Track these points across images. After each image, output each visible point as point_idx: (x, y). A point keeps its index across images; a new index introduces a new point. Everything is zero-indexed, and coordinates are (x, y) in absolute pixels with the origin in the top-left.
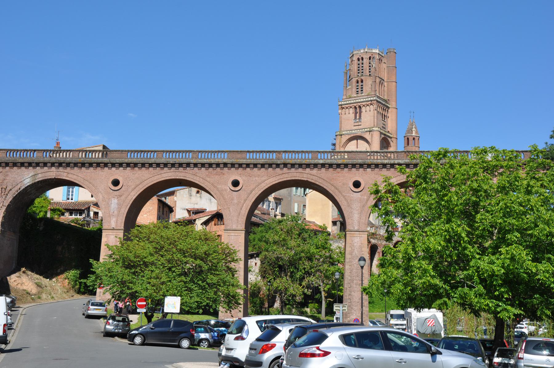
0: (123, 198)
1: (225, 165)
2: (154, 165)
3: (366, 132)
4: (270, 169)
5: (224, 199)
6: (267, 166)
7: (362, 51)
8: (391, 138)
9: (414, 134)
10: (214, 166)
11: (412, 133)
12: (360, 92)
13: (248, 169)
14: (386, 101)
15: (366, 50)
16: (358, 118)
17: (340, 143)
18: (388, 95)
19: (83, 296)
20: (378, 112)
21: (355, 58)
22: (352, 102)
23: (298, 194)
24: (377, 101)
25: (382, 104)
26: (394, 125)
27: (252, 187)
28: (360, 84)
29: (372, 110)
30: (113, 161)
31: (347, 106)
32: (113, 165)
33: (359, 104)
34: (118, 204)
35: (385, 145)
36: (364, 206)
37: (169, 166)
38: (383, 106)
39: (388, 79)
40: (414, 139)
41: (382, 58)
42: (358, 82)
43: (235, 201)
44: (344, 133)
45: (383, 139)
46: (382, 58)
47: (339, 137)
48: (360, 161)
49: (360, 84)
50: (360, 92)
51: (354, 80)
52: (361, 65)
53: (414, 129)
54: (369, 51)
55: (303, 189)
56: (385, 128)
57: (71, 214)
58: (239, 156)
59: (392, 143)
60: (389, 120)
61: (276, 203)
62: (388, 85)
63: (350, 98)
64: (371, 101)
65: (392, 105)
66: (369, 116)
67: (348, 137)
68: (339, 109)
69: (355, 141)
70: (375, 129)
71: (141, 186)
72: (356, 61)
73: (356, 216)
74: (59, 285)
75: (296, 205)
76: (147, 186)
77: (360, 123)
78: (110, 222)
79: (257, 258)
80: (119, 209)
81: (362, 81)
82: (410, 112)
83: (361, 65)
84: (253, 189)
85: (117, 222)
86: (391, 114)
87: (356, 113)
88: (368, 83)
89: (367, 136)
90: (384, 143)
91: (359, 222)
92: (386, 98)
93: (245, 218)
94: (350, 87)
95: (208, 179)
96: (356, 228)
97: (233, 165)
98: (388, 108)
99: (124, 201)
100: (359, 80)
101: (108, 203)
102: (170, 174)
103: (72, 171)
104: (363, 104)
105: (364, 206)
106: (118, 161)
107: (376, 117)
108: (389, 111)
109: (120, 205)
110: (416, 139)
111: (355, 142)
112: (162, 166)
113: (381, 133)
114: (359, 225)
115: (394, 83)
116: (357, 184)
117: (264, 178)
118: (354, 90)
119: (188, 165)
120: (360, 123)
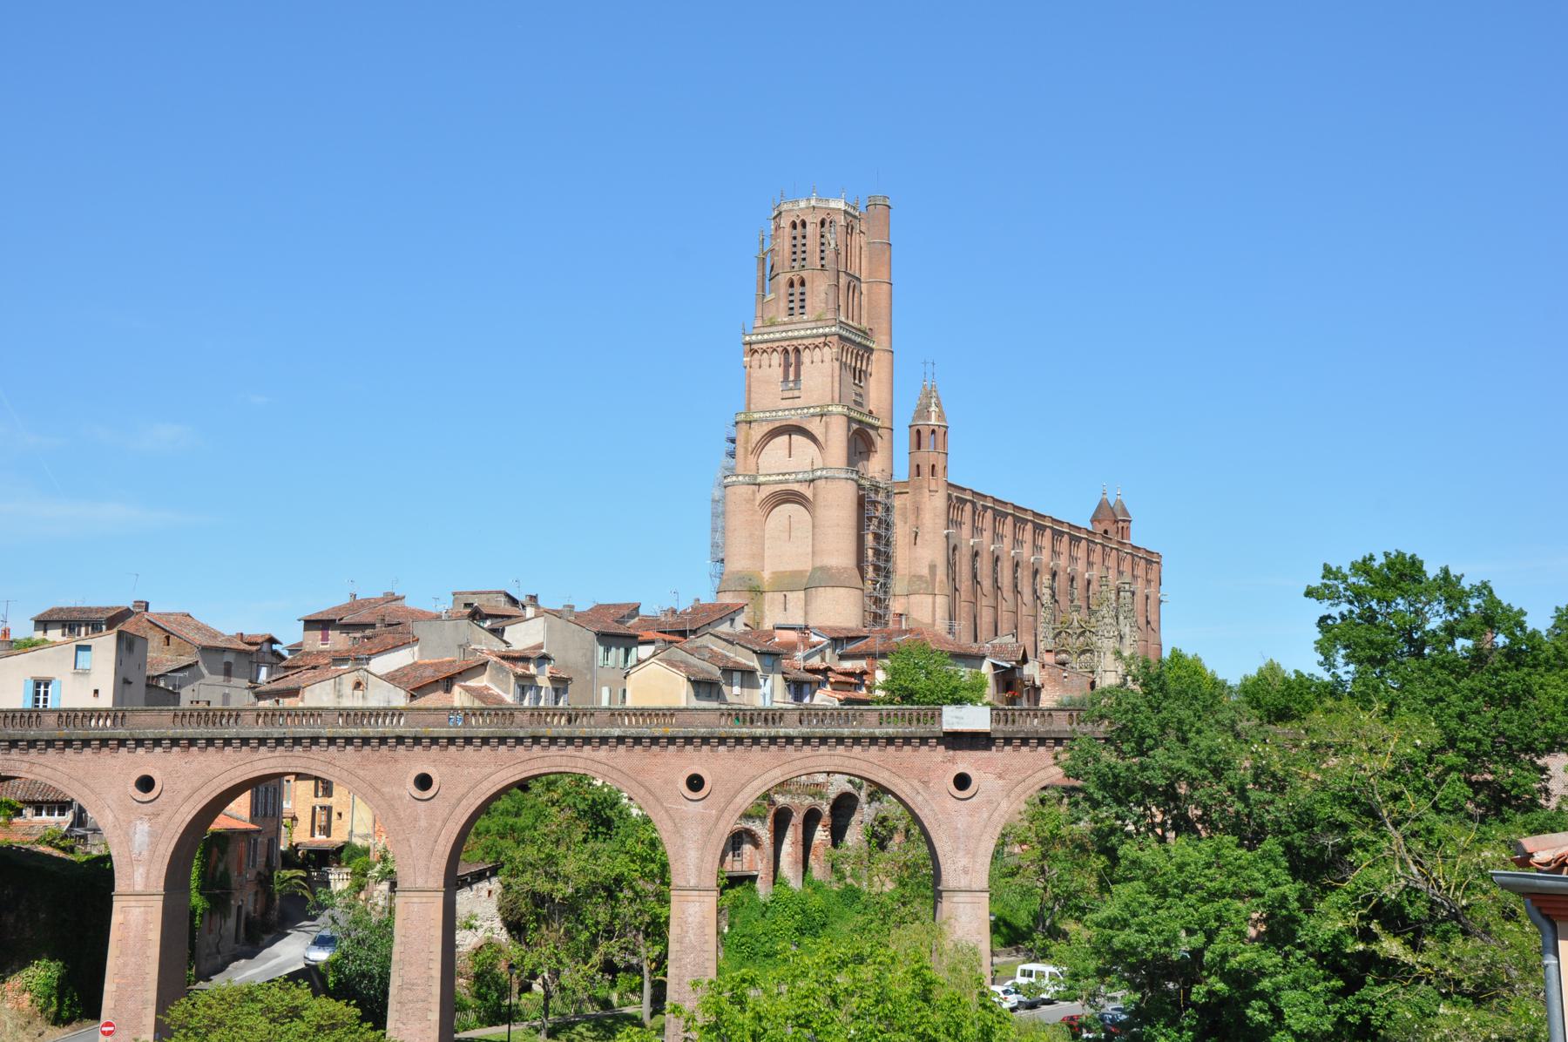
0: (161, 819)
1: (400, 740)
2: (236, 743)
3: (813, 415)
4: (502, 748)
5: (398, 818)
6: (494, 742)
7: (803, 204)
8: (876, 428)
9: (933, 421)
10: (375, 742)
11: (929, 418)
12: (797, 310)
13: (452, 749)
14: (865, 333)
15: (813, 203)
16: (792, 378)
17: (747, 442)
18: (870, 318)
19: (67, 1029)
20: (843, 365)
21: (785, 223)
22: (778, 336)
23: (611, 662)
24: (841, 337)
25: (853, 342)
26: (885, 395)
27: (462, 790)
28: (798, 289)
29: (827, 358)
30: (138, 733)
31: (764, 346)
32: (140, 742)
33: (795, 343)
34: (152, 834)
35: (861, 447)
36: (709, 833)
37: (271, 743)
38: (856, 350)
39: (870, 275)
40: (933, 432)
41: (856, 223)
42: (792, 285)
43: (423, 823)
44: (756, 416)
45: (855, 432)
46: (856, 223)
47: (744, 427)
48: (703, 731)
49: (798, 289)
50: (797, 310)
51: (783, 279)
52: (800, 241)
53: (933, 408)
54: (821, 205)
55: (622, 650)
56: (861, 405)
57: (39, 813)
58: (431, 718)
59: (878, 442)
60: (872, 380)
61: (556, 690)
62: (869, 291)
63: (773, 324)
64: (826, 335)
65: (879, 342)
66: (821, 373)
67: (766, 428)
68: (746, 354)
69: (785, 438)
70: (834, 409)
71: (204, 791)
72: (788, 229)
73: (692, 856)
74: (8, 1006)
75: (605, 692)
76: (219, 791)
77: (796, 393)
78: (131, 877)
79: (494, 880)
80: (153, 846)
81: (803, 284)
82: (925, 363)
83: (800, 241)
84: (464, 796)
85: (147, 877)
86: (878, 366)
87: (787, 366)
88: (819, 290)
89: (815, 426)
90: (859, 441)
91: (699, 870)
92: (865, 324)
93: (444, 862)
94: (773, 295)
95: (361, 773)
96: (692, 883)
97: (417, 740)
98: (870, 350)
99: (165, 827)
100: (796, 279)
101: (127, 833)
102: (272, 762)
103: (42, 759)
104: (806, 342)
105: (709, 833)
106: (151, 733)
107: (837, 379)
108: (873, 357)
109: (154, 837)
110: (940, 432)
111: (783, 440)
112: (254, 743)
113: (850, 420)
114: (699, 876)
115: (885, 287)
116: (695, 783)
117: (488, 770)
118: (783, 304)
119: (315, 740)
120: (796, 393)
